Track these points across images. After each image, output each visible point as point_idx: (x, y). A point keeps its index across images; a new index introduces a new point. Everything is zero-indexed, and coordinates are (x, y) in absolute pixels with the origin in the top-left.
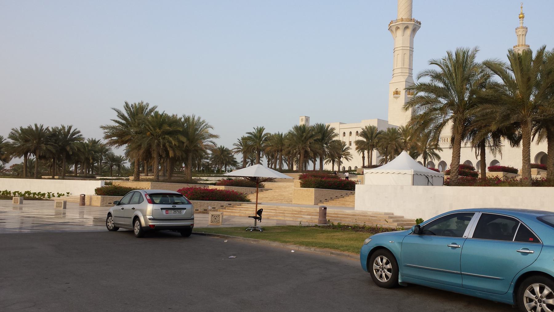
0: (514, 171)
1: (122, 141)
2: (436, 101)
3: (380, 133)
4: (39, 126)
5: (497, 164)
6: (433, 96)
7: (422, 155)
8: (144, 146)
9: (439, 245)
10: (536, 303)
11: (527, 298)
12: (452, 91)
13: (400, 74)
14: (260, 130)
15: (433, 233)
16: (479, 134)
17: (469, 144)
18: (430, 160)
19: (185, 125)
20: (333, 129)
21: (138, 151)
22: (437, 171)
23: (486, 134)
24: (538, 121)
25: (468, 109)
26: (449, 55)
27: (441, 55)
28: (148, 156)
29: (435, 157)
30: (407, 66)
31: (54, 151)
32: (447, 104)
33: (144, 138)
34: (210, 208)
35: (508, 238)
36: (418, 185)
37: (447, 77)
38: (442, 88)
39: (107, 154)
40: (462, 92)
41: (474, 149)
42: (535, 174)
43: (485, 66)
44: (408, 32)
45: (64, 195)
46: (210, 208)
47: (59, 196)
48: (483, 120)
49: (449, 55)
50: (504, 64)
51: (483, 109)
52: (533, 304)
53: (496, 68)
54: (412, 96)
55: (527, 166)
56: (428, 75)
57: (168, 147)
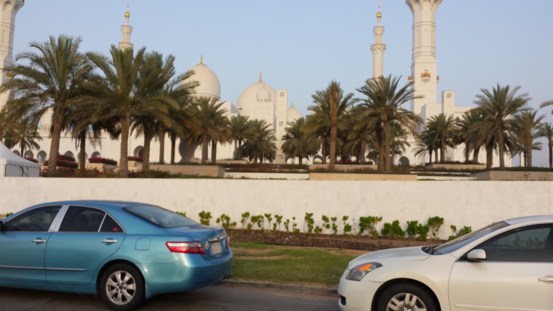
0: (113, 163)
2: (35, 87)
5: (98, 156)
6: (32, 81)
7: (19, 144)
9: (24, 241)
10: (117, 290)
11: (109, 286)
12: (53, 78)
15: (17, 229)
16: (79, 125)
17: (69, 135)
18: (28, 149)
22: (35, 161)
23: (86, 125)
24: (136, 117)
25: (69, 99)
26: (52, 40)
27: (43, 39)
29: (34, 146)
32: (47, 91)
35: (94, 229)
36: (8, 176)
37: (49, 63)
38: (43, 74)
40: (63, 81)
41: (74, 140)
42: (132, 167)
43: (88, 57)
44: (10, 8)
48: (84, 111)
49: (52, 40)
50: (107, 58)
51: (84, 100)
52: (114, 291)
53: (100, 62)
54: (10, 78)
55: (124, 159)
56: (27, 57)
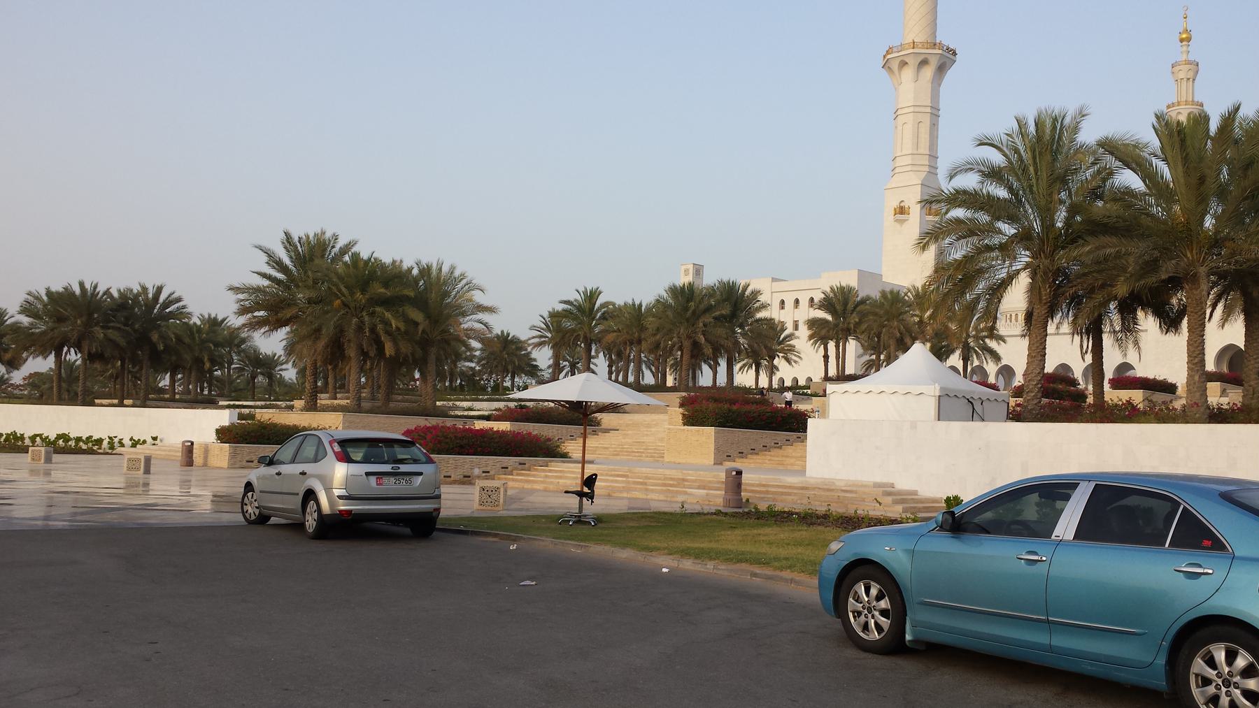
0: (1169, 388)
1: (278, 321)
2: (991, 230)
3: (863, 302)
4: (88, 286)
5: (1130, 373)
6: (983, 217)
7: (958, 352)
8: (328, 331)
9: (999, 555)
10: (1218, 687)
11: (1197, 675)
12: (1027, 206)
13: (909, 168)
14: (592, 296)
15: (984, 529)
16: (1088, 305)
17: (1066, 328)
18: (976, 363)
19: (421, 283)
20: (756, 293)
21: (314, 342)
22: (994, 387)
23: (1105, 304)
24: (1222, 276)
25: (1063, 248)
26: (1021, 124)
27: (1002, 126)
28: (336, 353)
29: (988, 357)
30: (924, 149)
31: (122, 342)
32: (1015, 235)
33: (327, 312)
34: (477, 471)
35: (1155, 540)
36: (950, 419)
37: (1016, 175)
38: (1005, 200)
39: (244, 351)
40: (1049, 210)
41: (1077, 338)
42: (1216, 396)
43: (1101, 150)
44: (928, 72)
45: (144, 442)
46: (477, 471)
47: (134, 445)
48: (1099, 272)
49: (1021, 124)
50: (1146, 145)
51: (1098, 248)
52: (1211, 690)
53: (1128, 155)
54: (937, 219)
55: (1197, 378)
56: (972, 169)
57: (382, 333)
